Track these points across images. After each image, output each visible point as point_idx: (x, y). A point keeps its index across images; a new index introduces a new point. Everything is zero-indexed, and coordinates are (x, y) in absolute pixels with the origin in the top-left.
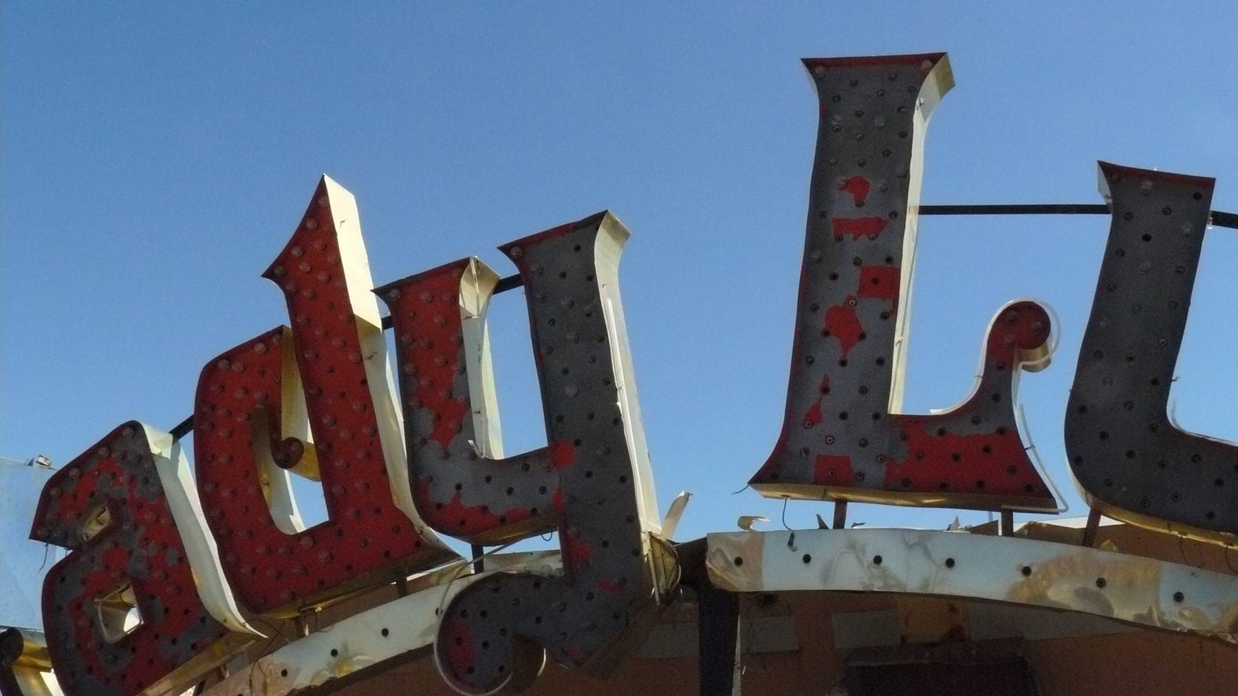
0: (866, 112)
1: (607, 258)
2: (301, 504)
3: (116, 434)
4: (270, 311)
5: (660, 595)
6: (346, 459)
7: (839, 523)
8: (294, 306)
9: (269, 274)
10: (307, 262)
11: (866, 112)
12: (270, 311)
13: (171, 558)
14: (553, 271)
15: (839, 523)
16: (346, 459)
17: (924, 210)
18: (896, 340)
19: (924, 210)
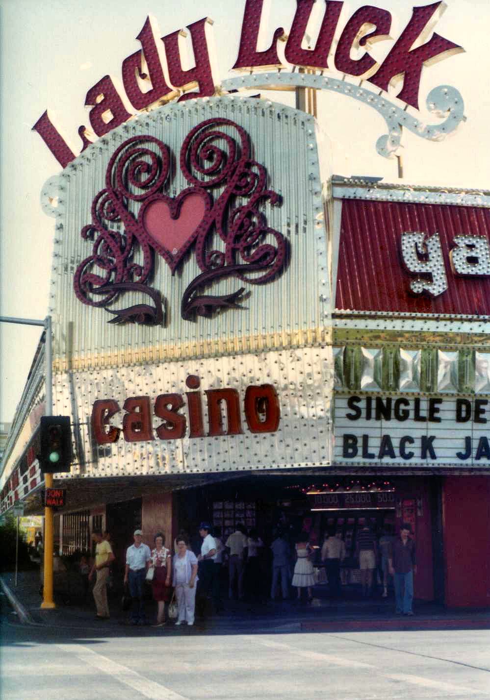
0: (44, 127)
1: (207, 27)
2: (145, 86)
3: (102, 81)
4: (137, 46)
5: (140, 252)
6: (156, 75)
7: (405, 110)
8: (143, 44)
9: (137, 38)
10: (145, 35)
11: (44, 127)
12: (137, 46)
13: (160, 69)
14: (197, 30)
15: (405, 110)
16: (156, 75)
17: (400, 175)
18: (195, 589)
19: (400, 175)
